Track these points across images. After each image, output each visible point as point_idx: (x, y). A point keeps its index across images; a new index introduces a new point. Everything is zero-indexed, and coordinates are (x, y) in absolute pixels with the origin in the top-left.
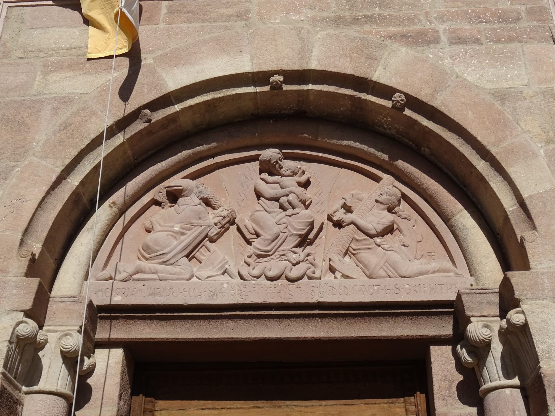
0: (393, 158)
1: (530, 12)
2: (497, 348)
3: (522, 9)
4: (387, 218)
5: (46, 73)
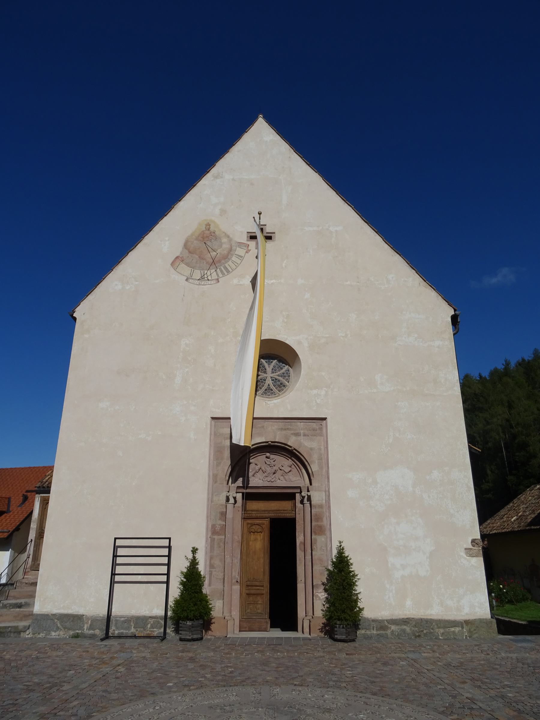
0: (291, 457)
1: (319, 428)
2: (306, 497)
3: (317, 427)
4: (290, 469)
5: (225, 440)
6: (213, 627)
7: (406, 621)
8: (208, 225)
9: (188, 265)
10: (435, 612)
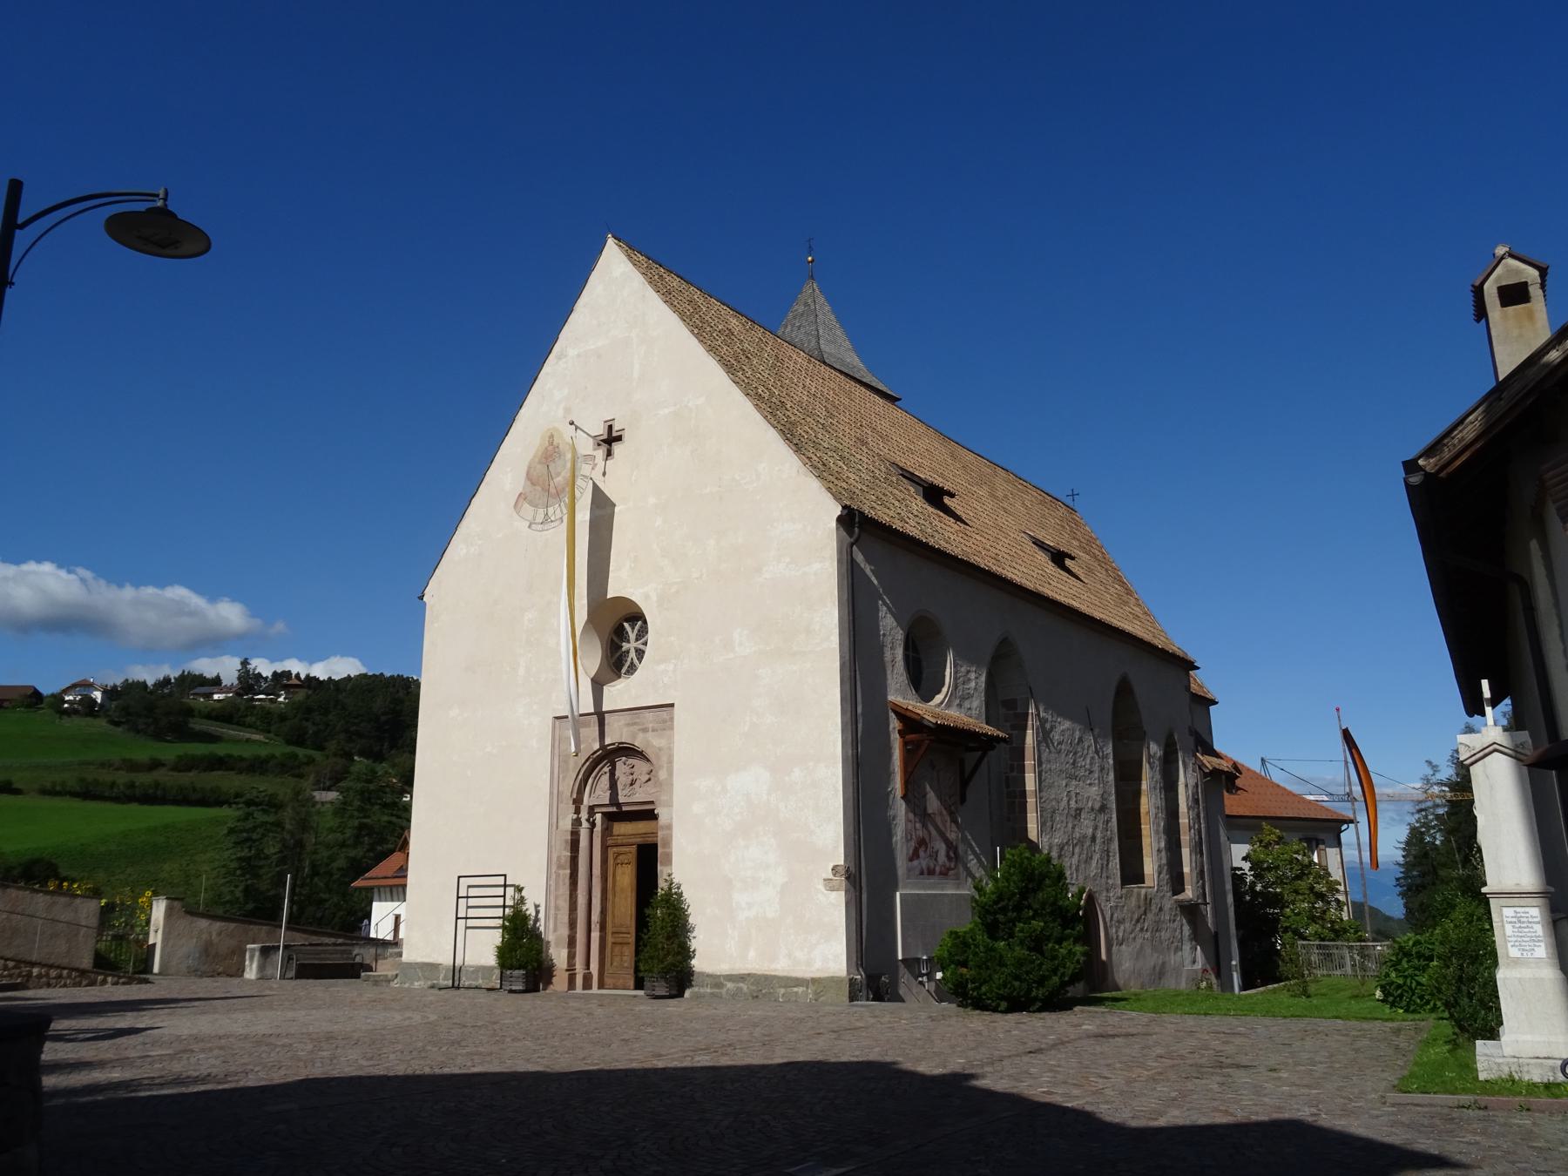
6: (554, 980)
7: (742, 978)
8: (552, 436)
9: (531, 503)
10: (781, 966)
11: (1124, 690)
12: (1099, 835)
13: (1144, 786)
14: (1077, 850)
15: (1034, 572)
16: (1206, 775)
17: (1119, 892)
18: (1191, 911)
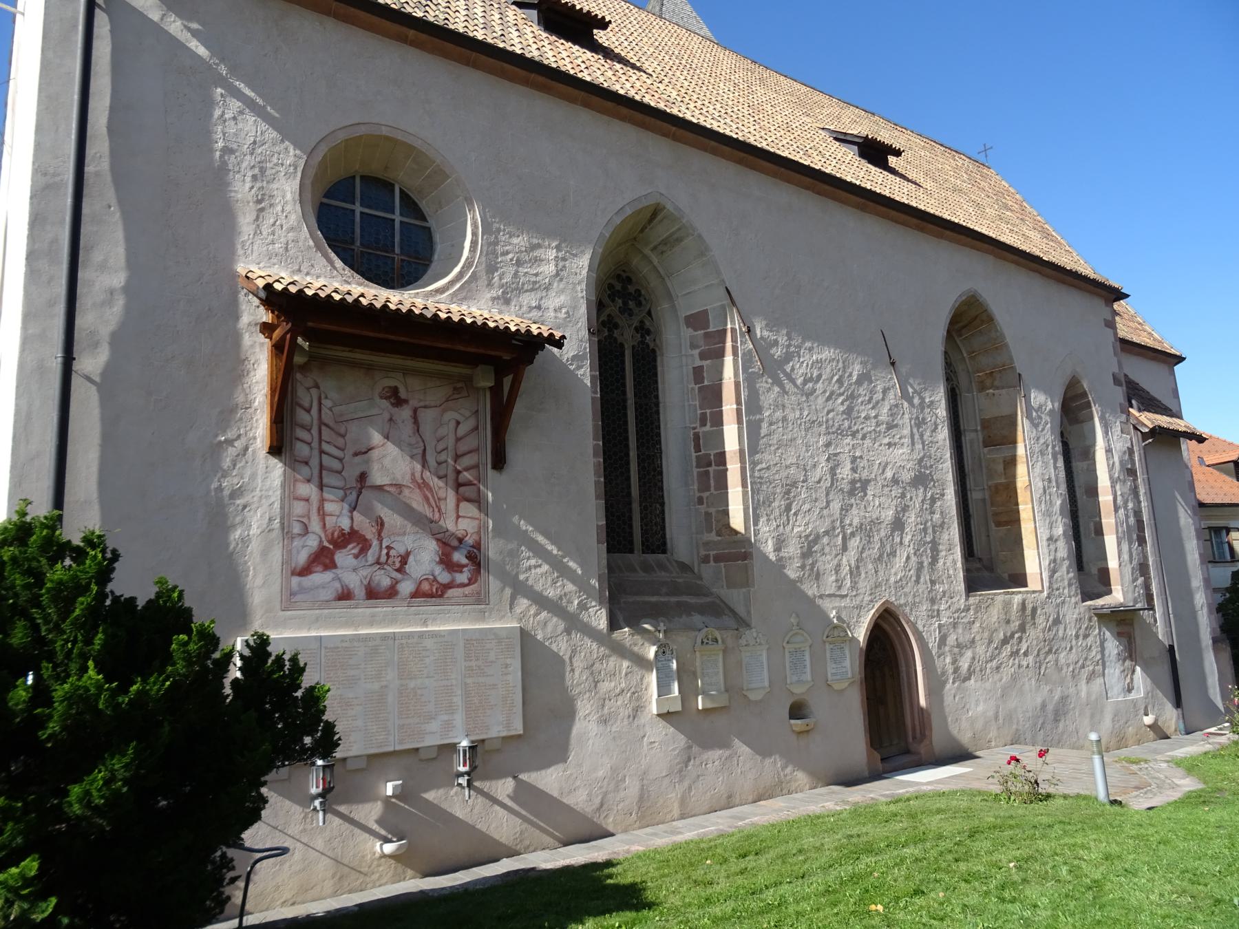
11: (968, 324)
12: (911, 518)
13: (1021, 450)
14: (854, 543)
15: (850, 167)
16: (1145, 436)
17: (961, 601)
18: (1123, 622)
